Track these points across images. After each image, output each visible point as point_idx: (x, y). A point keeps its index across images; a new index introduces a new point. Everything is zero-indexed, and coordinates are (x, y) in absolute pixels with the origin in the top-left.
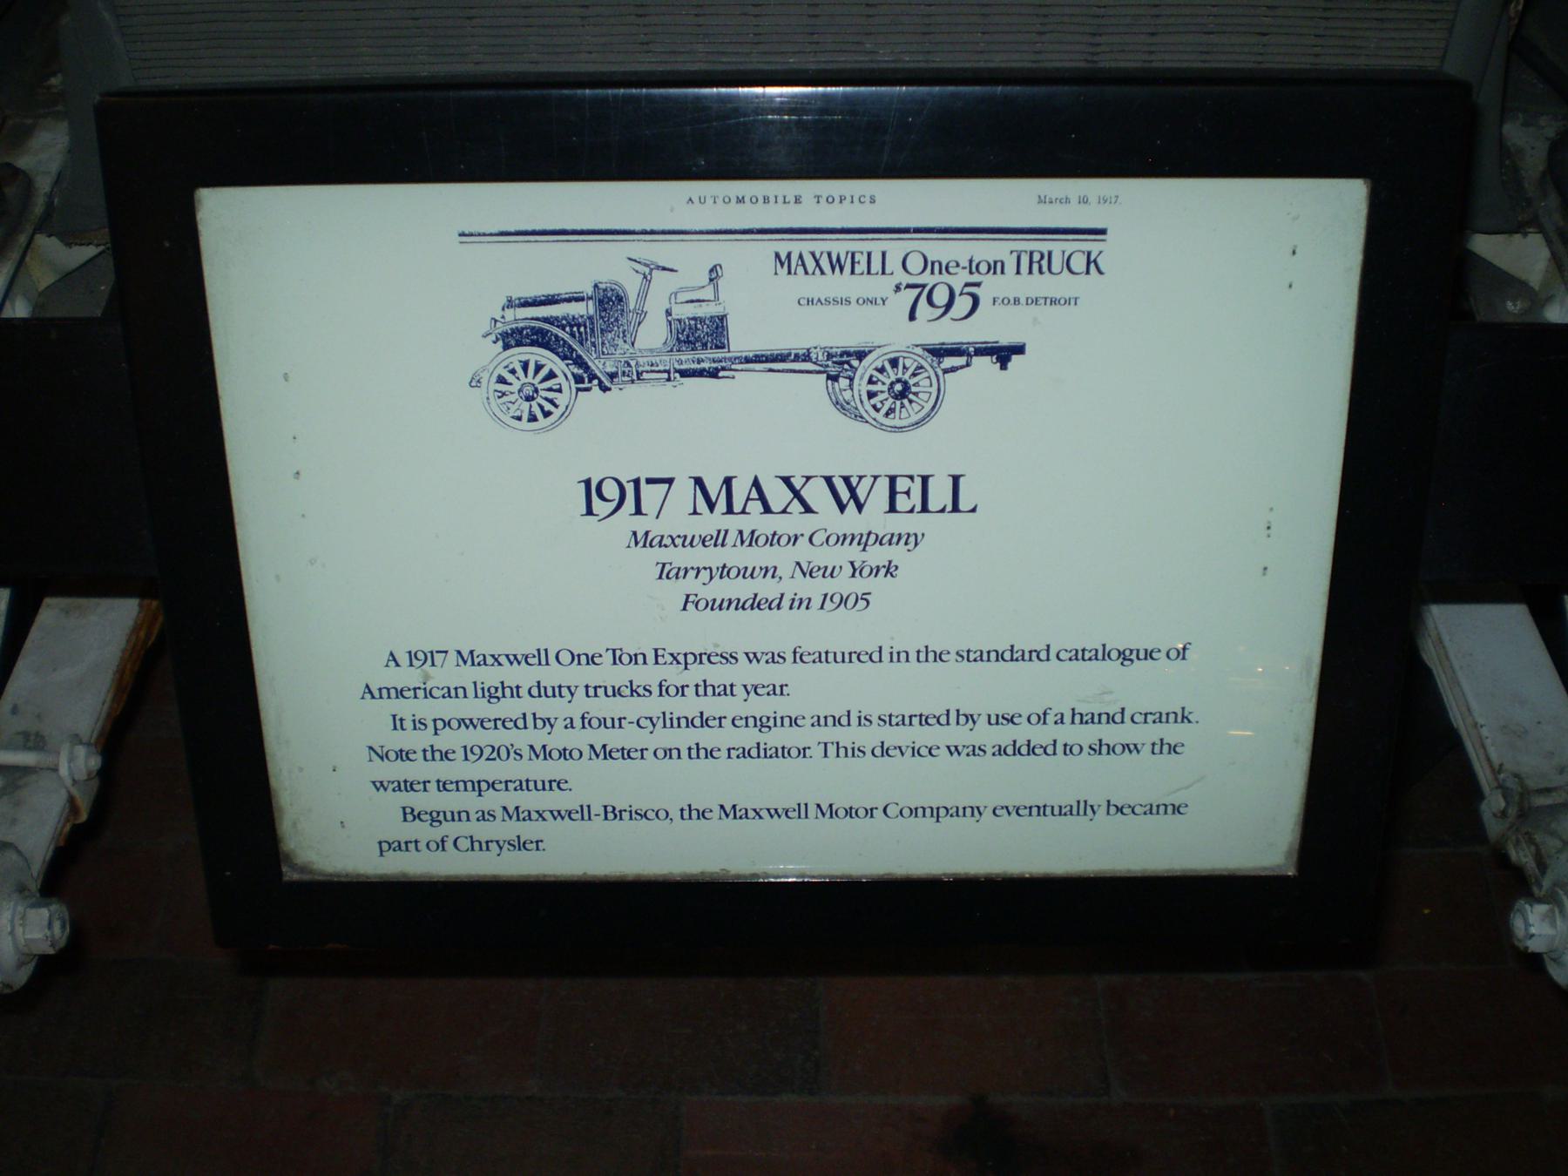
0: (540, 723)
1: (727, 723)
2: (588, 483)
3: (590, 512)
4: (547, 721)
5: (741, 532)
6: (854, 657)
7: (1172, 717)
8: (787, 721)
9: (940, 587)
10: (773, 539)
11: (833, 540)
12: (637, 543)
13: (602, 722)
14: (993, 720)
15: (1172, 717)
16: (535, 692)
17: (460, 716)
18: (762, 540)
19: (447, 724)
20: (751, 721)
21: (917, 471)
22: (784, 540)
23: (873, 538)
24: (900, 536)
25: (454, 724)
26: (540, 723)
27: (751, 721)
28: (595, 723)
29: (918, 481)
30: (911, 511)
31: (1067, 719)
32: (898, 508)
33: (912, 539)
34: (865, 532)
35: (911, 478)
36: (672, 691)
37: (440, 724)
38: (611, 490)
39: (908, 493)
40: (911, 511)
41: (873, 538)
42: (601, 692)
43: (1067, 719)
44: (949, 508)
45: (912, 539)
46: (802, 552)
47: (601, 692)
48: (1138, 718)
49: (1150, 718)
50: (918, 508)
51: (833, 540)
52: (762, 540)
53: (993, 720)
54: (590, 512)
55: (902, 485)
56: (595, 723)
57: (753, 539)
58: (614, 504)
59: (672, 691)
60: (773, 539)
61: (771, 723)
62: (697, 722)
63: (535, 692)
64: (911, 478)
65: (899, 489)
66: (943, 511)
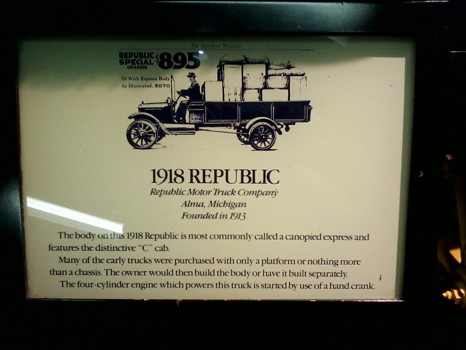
0: (291, 286)
1: (129, 286)
2: (154, 171)
3: (154, 182)
4: (294, 286)
5: (190, 190)
6: (71, 248)
7: (366, 286)
8: (151, 285)
9: (261, 213)
10: (202, 192)
11: (246, 193)
12: (191, 193)
13: (85, 285)
14: (302, 287)
15: (366, 286)
16: (98, 249)
17: (196, 283)
18: (197, 193)
19: (191, 286)
20: (138, 285)
21: (212, 168)
22: (205, 193)
23: (260, 192)
24: (270, 192)
25: (193, 286)
26: (291, 286)
27: (138, 285)
28: (82, 285)
29: (213, 172)
30: (211, 182)
31: (329, 287)
32: (206, 181)
33: (274, 193)
34: (257, 191)
35: (210, 170)
36: (281, 262)
37: (188, 286)
38: (162, 174)
39: (209, 176)
40: (211, 182)
41: (260, 192)
42: (134, 261)
43: (329, 287)
44: (262, 182)
45: (274, 193)
46: (212, 197)
47: (134, 261)
48: (354, 287)
49: (358, 287)
50: (213, 181)
51: (246, 193)
52: (197, 193)
53: (302, 287)
54: (154, 182)
55: (207, 173)
56: (82, 285)
57: (194, 192)
58: (163, 179)
59: (281, 262)
60: (202, 192)
61: (145, 286)
62: (119, 285)
63: (98, 249)
64: (210, 170)
65: (206, 174)
66: (260, 183)
